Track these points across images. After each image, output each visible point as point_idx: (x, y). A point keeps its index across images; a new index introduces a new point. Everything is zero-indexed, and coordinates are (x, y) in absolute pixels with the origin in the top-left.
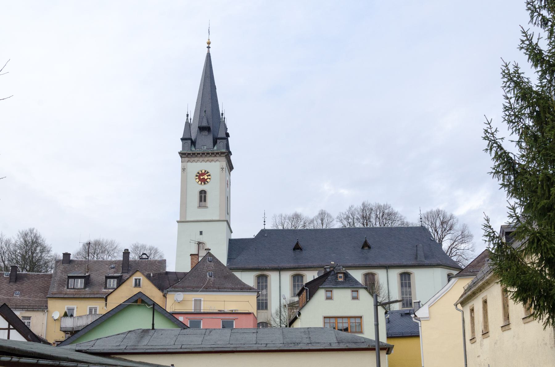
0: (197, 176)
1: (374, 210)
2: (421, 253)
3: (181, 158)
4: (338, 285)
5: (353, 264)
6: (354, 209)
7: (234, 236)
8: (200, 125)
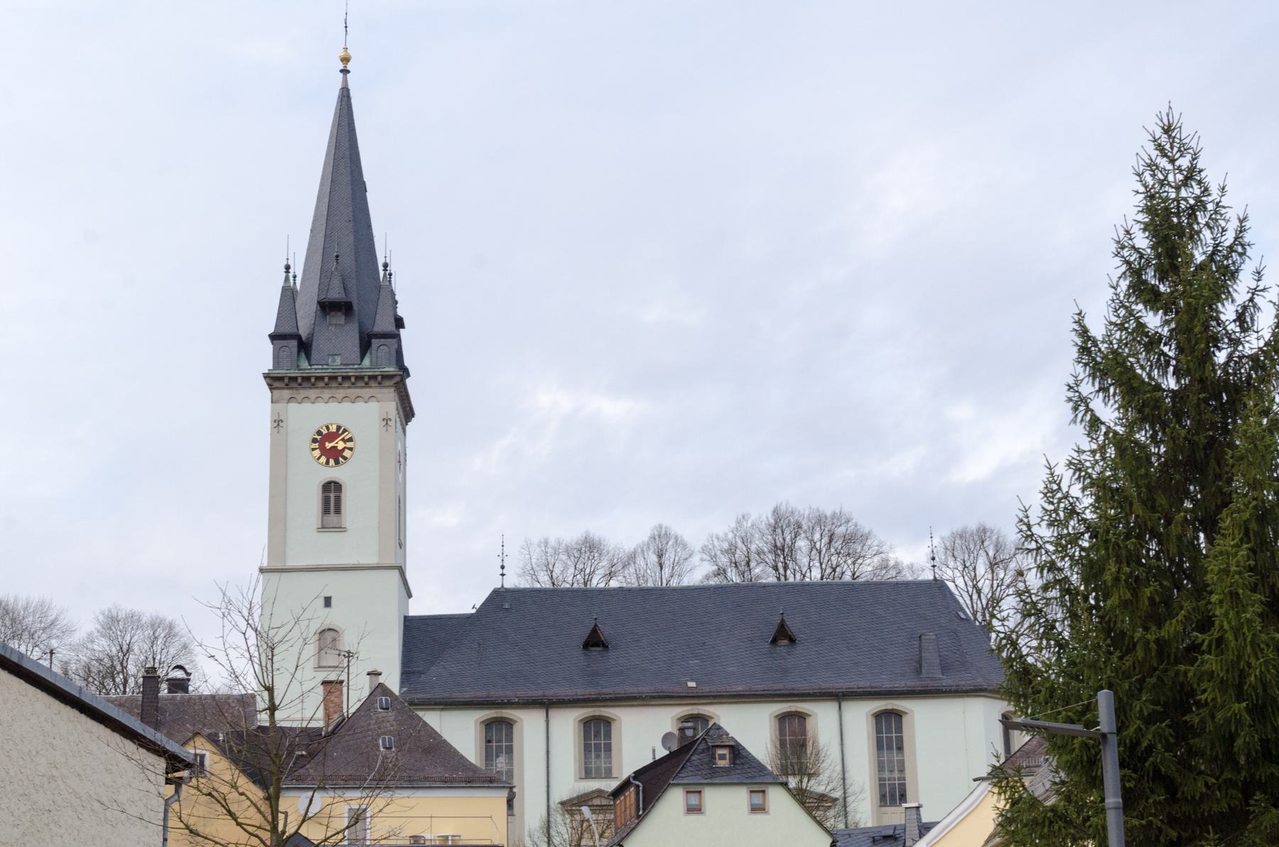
0: (314, 441)
1: (805, 527)
2: (931, 657)
3: (271, 389)
4: (715, 777)
5: (748, 688)
6: (749, 525)
7: (418, 608)
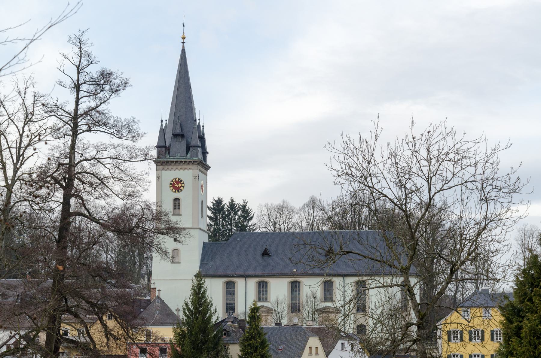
8: (174, 132)
